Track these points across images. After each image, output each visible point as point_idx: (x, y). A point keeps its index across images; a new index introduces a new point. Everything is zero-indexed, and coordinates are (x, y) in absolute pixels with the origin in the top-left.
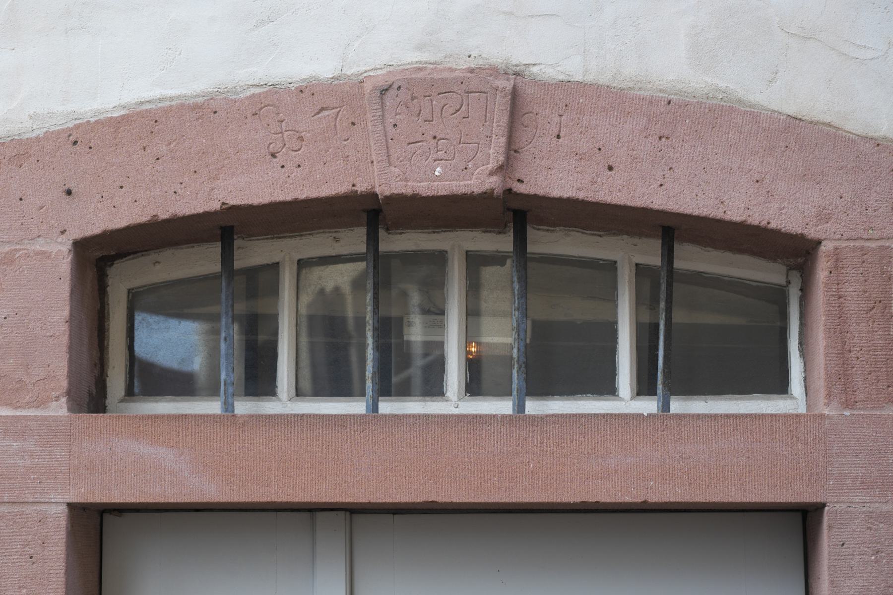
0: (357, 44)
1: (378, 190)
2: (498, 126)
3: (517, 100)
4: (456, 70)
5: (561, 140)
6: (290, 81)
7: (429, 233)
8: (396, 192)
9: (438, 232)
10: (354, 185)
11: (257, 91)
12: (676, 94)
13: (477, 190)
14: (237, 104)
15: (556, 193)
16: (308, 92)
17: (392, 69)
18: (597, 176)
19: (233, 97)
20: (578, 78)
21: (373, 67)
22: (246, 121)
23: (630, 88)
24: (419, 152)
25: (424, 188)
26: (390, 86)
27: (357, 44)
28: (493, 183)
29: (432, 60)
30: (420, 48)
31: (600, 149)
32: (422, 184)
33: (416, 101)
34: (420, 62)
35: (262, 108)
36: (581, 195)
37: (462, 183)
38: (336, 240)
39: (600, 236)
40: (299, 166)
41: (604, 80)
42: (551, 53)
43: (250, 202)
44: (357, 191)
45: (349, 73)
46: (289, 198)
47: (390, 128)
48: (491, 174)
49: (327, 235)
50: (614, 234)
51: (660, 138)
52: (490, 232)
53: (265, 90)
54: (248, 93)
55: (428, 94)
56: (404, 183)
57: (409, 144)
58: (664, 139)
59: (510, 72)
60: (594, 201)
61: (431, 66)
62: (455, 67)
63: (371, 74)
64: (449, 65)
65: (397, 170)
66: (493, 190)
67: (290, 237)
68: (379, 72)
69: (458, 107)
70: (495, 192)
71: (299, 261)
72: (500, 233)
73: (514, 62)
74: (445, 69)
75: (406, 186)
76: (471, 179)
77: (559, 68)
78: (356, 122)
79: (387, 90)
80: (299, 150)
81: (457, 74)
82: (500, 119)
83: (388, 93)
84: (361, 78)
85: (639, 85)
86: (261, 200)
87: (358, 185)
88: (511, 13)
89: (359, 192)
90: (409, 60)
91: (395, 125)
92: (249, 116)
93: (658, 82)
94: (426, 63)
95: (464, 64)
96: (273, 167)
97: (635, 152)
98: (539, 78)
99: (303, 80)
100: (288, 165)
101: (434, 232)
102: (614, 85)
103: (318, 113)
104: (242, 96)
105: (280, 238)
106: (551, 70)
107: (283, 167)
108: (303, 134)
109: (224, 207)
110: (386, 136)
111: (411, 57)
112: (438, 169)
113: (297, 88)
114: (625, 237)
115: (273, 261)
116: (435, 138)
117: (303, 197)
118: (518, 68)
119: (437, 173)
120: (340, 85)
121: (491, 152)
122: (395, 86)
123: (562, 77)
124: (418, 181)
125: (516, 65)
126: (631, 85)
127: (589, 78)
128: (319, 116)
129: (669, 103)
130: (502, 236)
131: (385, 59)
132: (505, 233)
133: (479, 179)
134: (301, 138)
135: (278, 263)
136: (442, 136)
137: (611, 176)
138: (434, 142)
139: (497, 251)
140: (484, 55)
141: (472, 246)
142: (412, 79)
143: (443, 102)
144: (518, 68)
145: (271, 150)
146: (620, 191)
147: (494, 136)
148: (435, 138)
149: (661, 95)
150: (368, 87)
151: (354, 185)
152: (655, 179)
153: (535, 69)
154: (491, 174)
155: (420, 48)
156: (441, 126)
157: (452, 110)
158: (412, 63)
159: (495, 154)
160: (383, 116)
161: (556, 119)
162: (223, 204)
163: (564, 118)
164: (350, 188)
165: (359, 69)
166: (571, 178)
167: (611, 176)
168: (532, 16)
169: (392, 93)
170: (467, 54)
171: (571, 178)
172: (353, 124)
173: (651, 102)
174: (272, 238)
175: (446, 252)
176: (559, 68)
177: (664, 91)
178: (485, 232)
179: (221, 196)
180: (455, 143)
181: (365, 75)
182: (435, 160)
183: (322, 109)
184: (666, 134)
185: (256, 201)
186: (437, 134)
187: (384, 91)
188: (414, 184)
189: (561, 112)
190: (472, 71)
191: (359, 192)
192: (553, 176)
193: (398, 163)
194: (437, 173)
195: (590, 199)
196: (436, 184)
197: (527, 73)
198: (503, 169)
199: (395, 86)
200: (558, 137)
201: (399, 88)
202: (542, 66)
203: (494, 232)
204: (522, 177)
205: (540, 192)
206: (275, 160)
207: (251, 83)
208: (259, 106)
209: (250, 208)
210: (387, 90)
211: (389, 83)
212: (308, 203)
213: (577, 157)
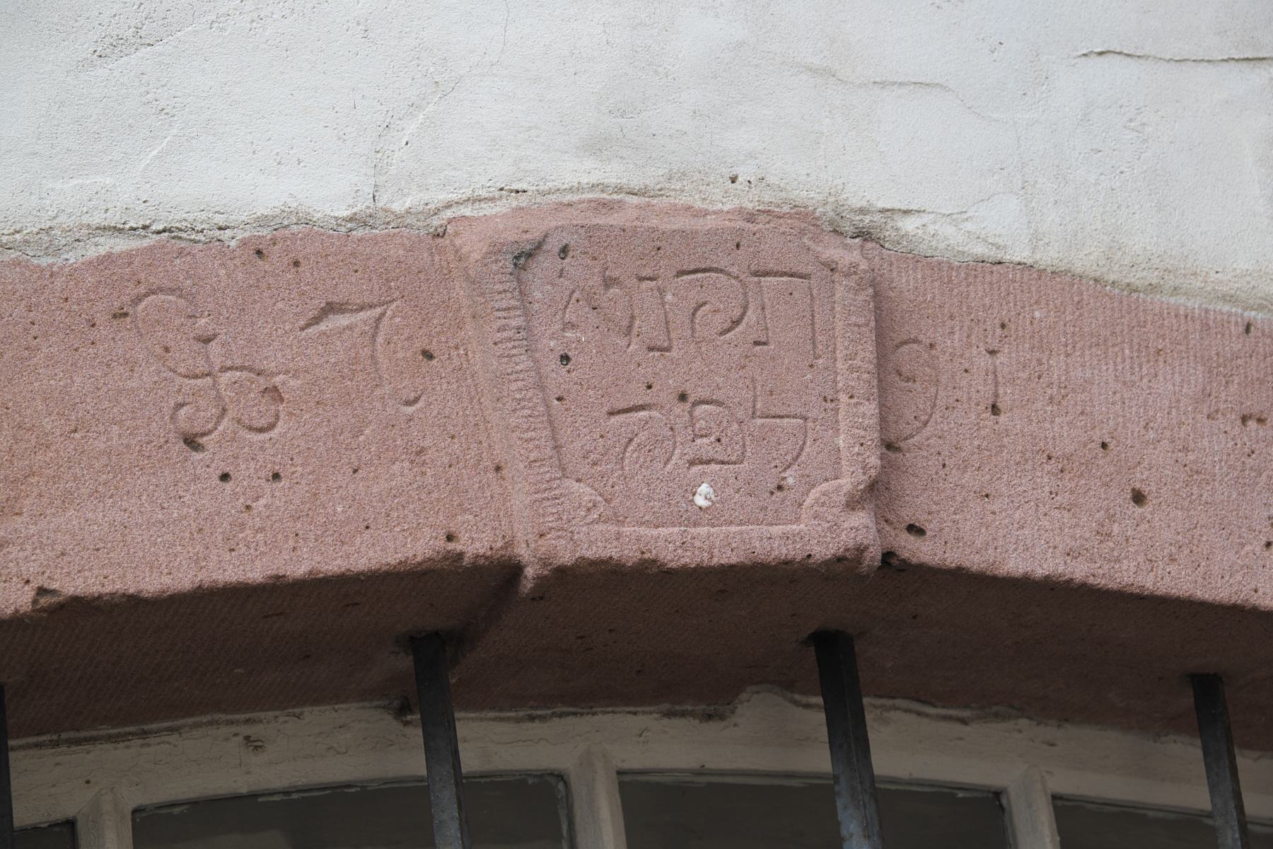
0: (412, 127)
1: (523, 552)
2: (852, 369)
3: (879, 302)
4: (706, 213)
5: (1002, 418)
6: (220, 220)
7: (518, 720)
8: (590, 554)
9: (542, 718)
10: (450, 538)
11: (121, 245)
12: (1261, 308)
13: (823, 549)
14: (59, 282)
15: (1014, 564)
16: (277, 251)
17: (523, 200)
18: (1111, 518)
19: (45, 261)
20: (1019, 253)
21: (468, 193)
22: (93, 334)
23: (1152, 288)
24: (642, 436)
25: (672, 544)
26: (539, 246)
27: (412, 127)
28: (857, 530)
29: (636, 183)
30: (595, 147)
31: (1104, 446)
32: (663, 531)
33: (615, 291)
34: (603, 188)
35: (138, 300)
36: (1079, 571)
37: (777, 530)
38: (253, 744)
39: (963, 721)
40: (276, 476)
41: (1086, 260)
42: (956, 178)
43: (131, 587)
44: (461, 555)
45: (397, 207)
46: (256, 573)
47: (551, 364)
48: (852, 504)
49: (224, 730)
50: (996, 715)
51: (1244, 419)
52: (683, 714)
53: (146, 243)
54: (92, 252)
55: (647, 272)
56: (613, 528)
57: (611, 413)
58: (1252, 424)
59: (849, 229)
60: (1112, 585)
61: (635, 200)
62: (699, 204)
63: (467, 211)
64: (683, 200)
65: (583, 488)
66: (861, 550)
67: (110, 739)
68: (487, 210)
69: (737, 312)
70: (867, 555)
71: (135, 811)
72: (709, 717)
73: (856, 203)
74: (675, 210)
75: (618, 536)
76: (798, 520)
77: (969, 226)
78: (433, 348)
79: (530, 255)
80: (271, 427)
81: (711, 222)
82: (851, 358)
83: (533, 264)
84: (436, 222)
85: (1171, 281)
86: (167, 580)
87: (464, 537)
88: (829, 73)
89: (466, 561)
90: (570, 180)
91: (565, 358)
92: (100, 319)
93: (1213, 276)
94: (619, 189)
95: (723, 200)
96: (196, 478)
97: (1191, 457)
98: (923, 249)
99: (262, 221)
100: (242, 472)
101: (532, 718)
102: (1112, 277)
103: (316, 320)
104: (72, 257)
105: (78, 742)
106: (949, 230)
107: (225, 477)
108: (278, 380)
109: (43, 601)
110: (542, 388)
111: (575, 173)
112: (704, 488)
113: (244, 243)
114: (1024, 722)
115: (59, 815)
116: (683, 397)
117: (298, 569)
118: (867, 219)
119: (700, 501)
120: (375, 241)
121: (841, 442)
122: (554, 245)
123: (979, 250)
124: (646, 523)
125: (862, 211)
126: (1153, 278)
127: (1048, 257)
128: (322, 327)
129: (1248, 329)
130: (713, 727)
131: (500, 172)
132: (722, 717)
133: (815, 522)
134: (274, 393)
135: (70, 824)
136: (703, 393)
137: (1143, 518)
138: (680, 409)
139: (701, 772)
140: (771, 179)
141: (634, 757)
142: (598, 227)
143: (695, 296)
144: (867, 219)
145: (183, 425)
146: (1173, 560)
147: (843, 398)
148: (683, 397)
149: (1226, 308)
150: (473, 246)
151: (450, 538)
152: (1250, 529)
153: (909, 225)
154: (852, 504)
155: (595, 147)
156: (697, 365)
157: (719, 321)
158: (579, 189)
159: (850, 451)
160: (528, 329)
161: (984, 361)
162: (42, 591)
163: (1001, 358)
164: (441, 544)
165: (426, 197)
166: (1045, 523)
167: (1143, 518)
168: (883, 84)
169: (546, 264)
170: (728, 173)
171: (1045, 523)
172: (428, 355)
173: (1206, 327)
174: (55, 744)
175: (561, 777)
176: (969, 226)
177: (1229, 298)
178: (669, 714)
179: (33, 568)
180: (740, 414)
181: (449, 214)
182: (692, 463)
183: (330, 309)
184: (1256, 410)
185: (151, 583)
186: (688, 387)
187: (525, 257)
188: (643, 530)
189: (994, 345)
190: (751, 217)
191: (466, 561)
192: (1011, 522)
193: (584, 469)
194: (700, 501)
195: (1101, 582)
196: (703, 530)
197: (889, 233)
198: (876, 493)
199: (554, 245)
200: (995, 410)
201: (564, 251)
202: (926, 218)
203: (692, 714)
204: (920, 519)
205: (975, 561)
206: (197, 456)
207: (97, 219)
208: (132, 291)
209: (133, 607)
210: (530, 255)
211: (536, 235)
212: (278, 595)
213: (1052, 466)
